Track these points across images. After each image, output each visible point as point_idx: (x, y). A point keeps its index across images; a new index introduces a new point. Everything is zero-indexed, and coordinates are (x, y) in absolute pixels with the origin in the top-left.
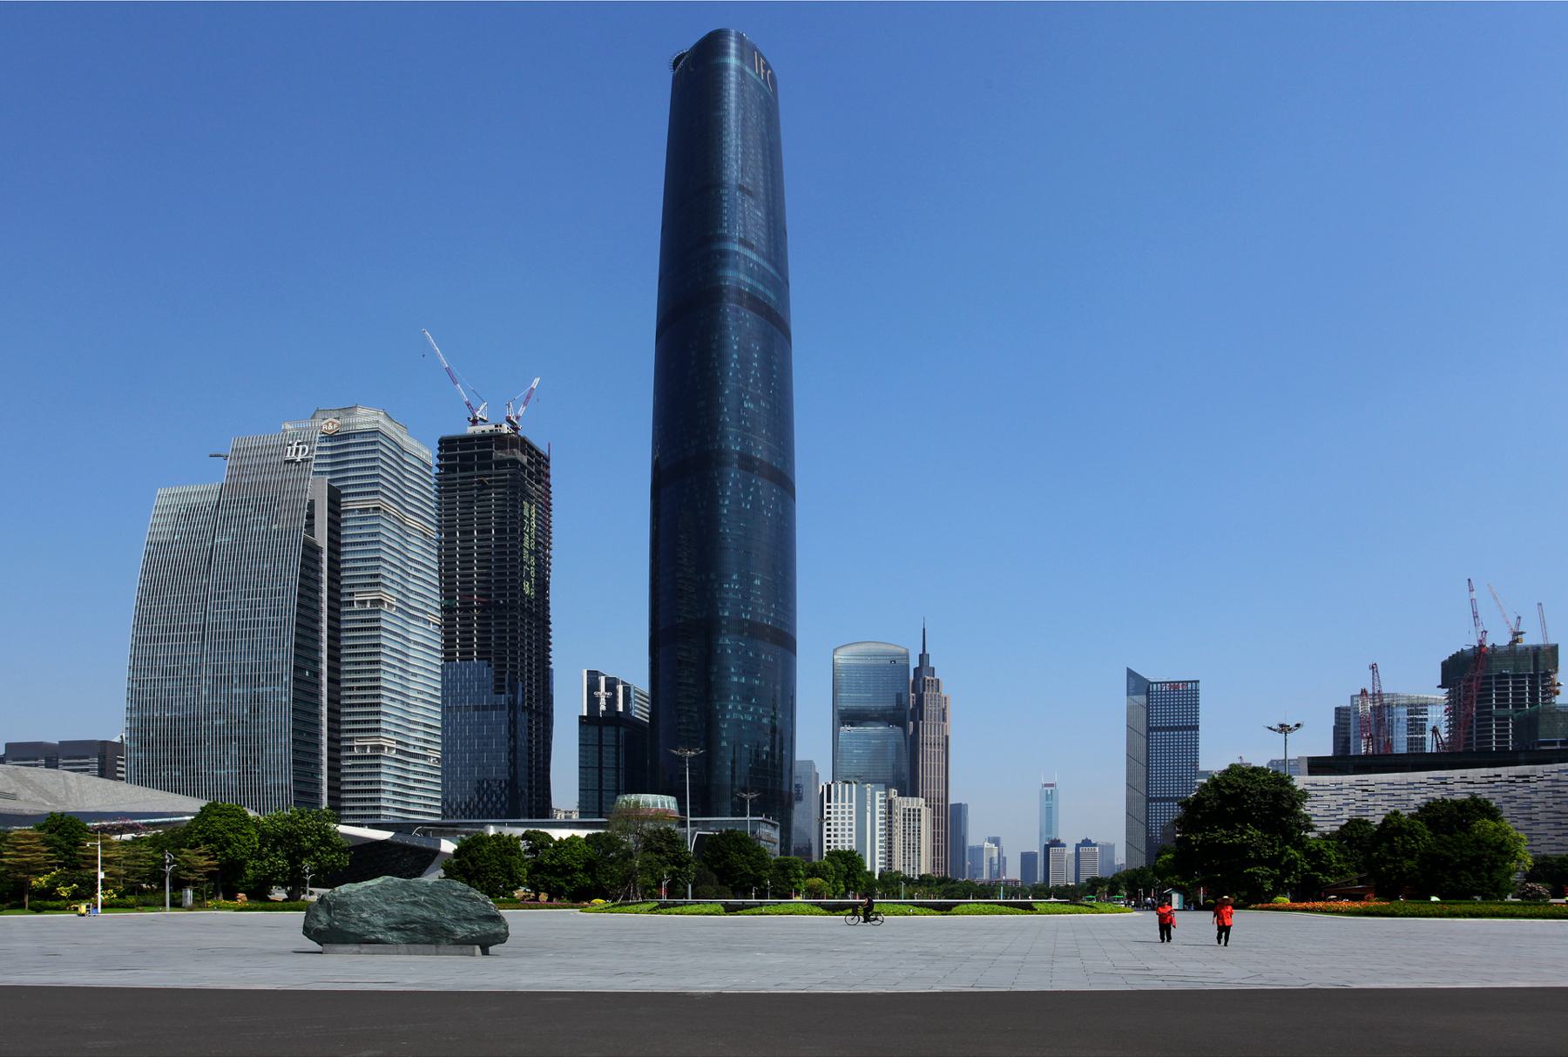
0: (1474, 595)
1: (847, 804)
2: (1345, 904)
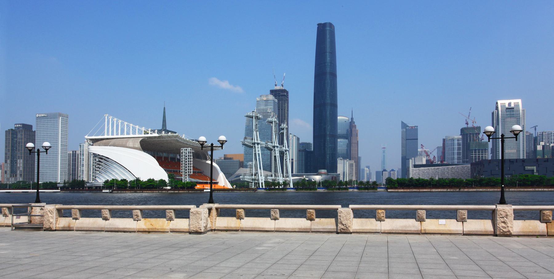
0: (470, 111)
1: (341, 165)
2: (76, 191)
